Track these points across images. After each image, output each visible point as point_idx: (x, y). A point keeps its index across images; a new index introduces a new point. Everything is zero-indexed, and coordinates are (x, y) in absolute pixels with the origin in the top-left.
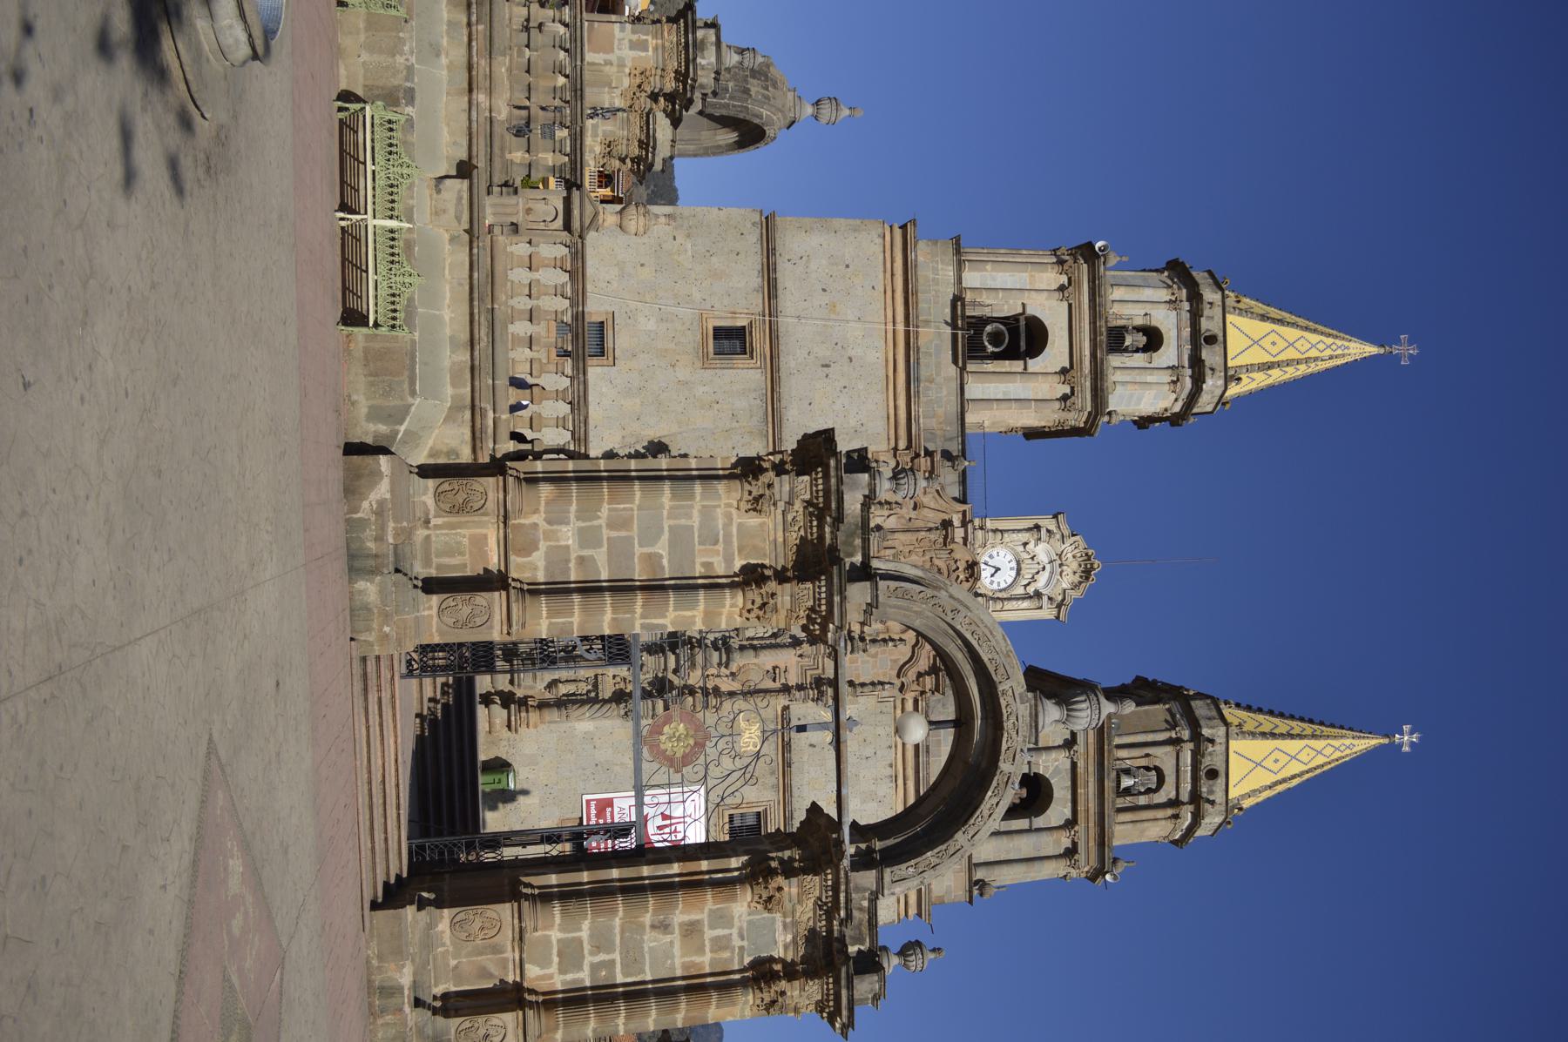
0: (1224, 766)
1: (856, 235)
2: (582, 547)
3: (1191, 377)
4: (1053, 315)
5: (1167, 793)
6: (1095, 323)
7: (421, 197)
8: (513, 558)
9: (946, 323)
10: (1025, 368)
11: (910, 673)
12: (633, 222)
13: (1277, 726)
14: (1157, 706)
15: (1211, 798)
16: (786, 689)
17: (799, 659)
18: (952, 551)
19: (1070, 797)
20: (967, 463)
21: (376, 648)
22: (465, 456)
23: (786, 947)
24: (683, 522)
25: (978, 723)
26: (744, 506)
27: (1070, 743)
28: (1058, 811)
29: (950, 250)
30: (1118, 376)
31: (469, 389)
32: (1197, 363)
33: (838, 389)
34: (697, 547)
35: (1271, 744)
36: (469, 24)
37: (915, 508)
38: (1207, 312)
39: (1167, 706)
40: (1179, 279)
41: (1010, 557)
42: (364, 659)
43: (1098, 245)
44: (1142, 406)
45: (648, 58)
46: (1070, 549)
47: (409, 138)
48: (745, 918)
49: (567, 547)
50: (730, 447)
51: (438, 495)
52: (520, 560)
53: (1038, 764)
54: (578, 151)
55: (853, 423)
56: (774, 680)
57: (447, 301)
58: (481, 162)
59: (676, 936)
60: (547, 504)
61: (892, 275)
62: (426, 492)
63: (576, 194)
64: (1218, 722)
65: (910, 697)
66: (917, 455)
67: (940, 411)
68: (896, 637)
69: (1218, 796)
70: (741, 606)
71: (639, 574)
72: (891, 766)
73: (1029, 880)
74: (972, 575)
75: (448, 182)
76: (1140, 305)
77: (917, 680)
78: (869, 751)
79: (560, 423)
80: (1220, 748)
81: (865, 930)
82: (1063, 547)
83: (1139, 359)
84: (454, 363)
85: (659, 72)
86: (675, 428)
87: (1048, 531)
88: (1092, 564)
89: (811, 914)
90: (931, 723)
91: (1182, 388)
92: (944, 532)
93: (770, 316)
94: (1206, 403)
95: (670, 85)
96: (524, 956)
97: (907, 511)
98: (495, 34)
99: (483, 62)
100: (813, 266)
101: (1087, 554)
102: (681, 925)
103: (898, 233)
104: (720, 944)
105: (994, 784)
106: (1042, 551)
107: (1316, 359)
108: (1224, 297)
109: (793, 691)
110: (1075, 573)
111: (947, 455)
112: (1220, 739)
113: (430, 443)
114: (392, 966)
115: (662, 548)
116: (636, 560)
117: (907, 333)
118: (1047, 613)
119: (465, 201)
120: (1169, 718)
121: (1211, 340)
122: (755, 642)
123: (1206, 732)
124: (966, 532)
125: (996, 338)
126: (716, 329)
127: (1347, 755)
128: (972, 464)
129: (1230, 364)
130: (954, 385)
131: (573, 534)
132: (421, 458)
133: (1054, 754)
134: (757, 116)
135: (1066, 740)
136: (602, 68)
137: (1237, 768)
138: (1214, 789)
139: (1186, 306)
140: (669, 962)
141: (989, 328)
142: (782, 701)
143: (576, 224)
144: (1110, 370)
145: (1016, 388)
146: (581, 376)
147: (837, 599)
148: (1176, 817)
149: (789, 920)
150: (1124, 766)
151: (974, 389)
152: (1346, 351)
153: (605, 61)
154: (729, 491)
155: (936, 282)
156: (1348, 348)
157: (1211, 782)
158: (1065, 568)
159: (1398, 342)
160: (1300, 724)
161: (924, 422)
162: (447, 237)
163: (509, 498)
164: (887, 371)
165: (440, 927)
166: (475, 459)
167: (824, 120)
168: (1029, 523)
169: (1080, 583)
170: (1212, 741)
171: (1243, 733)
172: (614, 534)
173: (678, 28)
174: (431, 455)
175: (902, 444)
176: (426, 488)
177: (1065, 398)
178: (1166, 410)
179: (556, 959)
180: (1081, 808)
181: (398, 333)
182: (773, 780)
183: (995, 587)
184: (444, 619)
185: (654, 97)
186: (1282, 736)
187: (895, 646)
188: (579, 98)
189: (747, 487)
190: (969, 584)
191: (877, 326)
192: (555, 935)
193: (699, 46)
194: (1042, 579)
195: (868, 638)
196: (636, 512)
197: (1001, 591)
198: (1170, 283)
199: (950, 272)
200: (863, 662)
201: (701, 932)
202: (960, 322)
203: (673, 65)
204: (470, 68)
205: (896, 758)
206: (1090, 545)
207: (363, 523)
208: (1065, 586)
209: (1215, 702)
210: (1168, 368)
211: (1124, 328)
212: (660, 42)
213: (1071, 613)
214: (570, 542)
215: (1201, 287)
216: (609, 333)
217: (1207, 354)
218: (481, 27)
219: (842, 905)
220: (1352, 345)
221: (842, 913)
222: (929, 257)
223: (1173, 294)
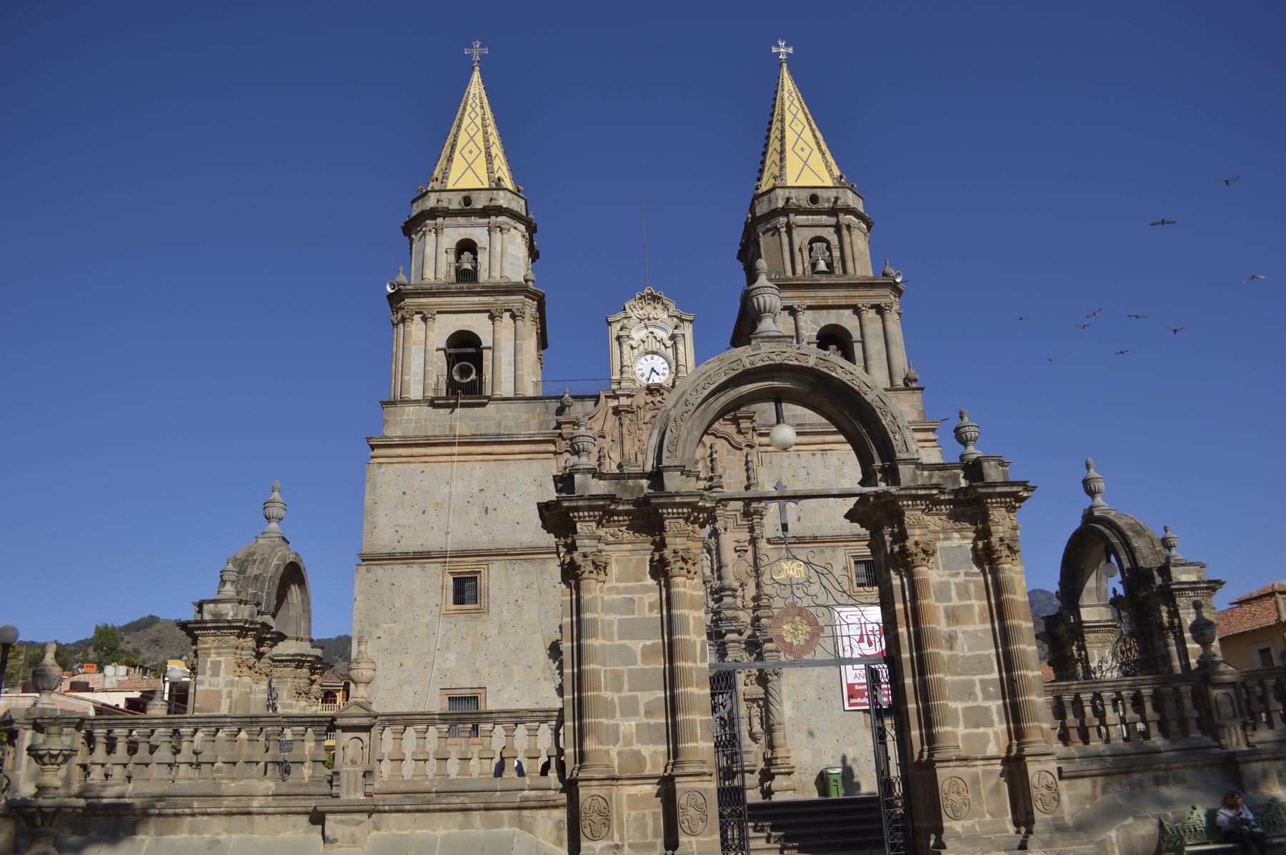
0: (807, 190)
1: (378, 486)
2: (636, 713)
3: (497, 217)
4: (446, 326)
5: (829, 234)
6: (453, 293)
8: (647, 772)
9: (452, 412)
10: (489, 348)
12: (364, 672)
13: (775, 149)
14: (761, 242)
15: (833, 200)
16: (753, 541)
19: (835, 311)
20: (567, 395)
22: (561, 814)
23: (964, 538)
24: (615, 628)
25: (776, 384)
26: (602, 577)
27: (792, 311)
28: (847, 320)
31: (504, 812)
32: (486, 212)
33: (507, 500)
34: (636, 615)
37: (603, 437)
38: (445, 204)
39: (761, 235)
40: (418, 226)
41: (642, 360)
43: (389, 290)
44: (520, 255)
45: (226, 661)
46: (636, 312)
48: (941, 571)
49: (637, 726)
50: (554, 589)
51: (594, 838)
52: (649, 766)
54: (303, 720)
55: (533, 488)
56: (746, 551)
57: (429, 832)
58: (311, 804)
59: (959, 629)
60: (601, 744)
63: (339, 722)
64: (772, 195)
66: (560, 435)
67: (524, 417)
68: (709, 451)
69: (832, 194)
71: (659, 665)
72: (814, 455)
75: (327, 832)
76: (439, 257)
79: (533, 733)
80: (794, 194)
81: (947, 473)
82: (634, 317)
83: (482, 258)
84: (483, 826)
85: (238, 651)
86: (538, 636)
87: (621, 329)
88: (648, 294)
89: (936, 518)
91: (506, 223)
92: (623, 413)
93: (446, 557)
94: (518, 205)
95: (250, 642)
96: (980, 756)
97: (606, 443)
100: (404, 522)
101: (640, 299)
102: (949, 625)
103: (378, 452)
104: (963, 592)
105: (825, 370)
106: (638, 334)
107: (483, 119)
109: (755, 535)
110: (655, 308)
111: (560, 411)
112: (787, 193)
115: (637, 646)
116: (648, 667)
117: (461, 444)
118: (687, 330)
120: (771, 233)
121: (467, 201)
122: (715, 567)
123: (781, 204)
124: (623, 395)
125: (465, 372)
126: (456, 602)
128: (567, 390)
129: (487, 186)
130: (503, 405)
131: (627, 721)
133: (801, 324)
135: (790, 314)
138: (825, 197)
139: (440, 220)
140: (979, 634)
142: (762, 544)
143: (365, 721)
144: (491, 280)
145: (505, 356)
146: (493, 716)
147: (678, 500)
148: (848, 227)
150: (809, 268)
151: (506, 389)
152: (477, 96)
153: (228, 698)
154: (589, 590)
155: (417, 421)
156: (475, 95)
157: (820, 200)
158: (651, 316)
159: (470, 56)
160: (773, 131)
162: (374, 833)
167: (282, 513)
168: (615, 344)
169: (663, 304)
170: (788, 200)
171: (781, 175)
172: (626, 686)
173: (202, 635)
174: (561, 844)
175: (551, 448)
176: (588, 848)
177: (513, 317)
178: (523, 236)
179: (982, 730)
180: (844, 302)
182: (828, 551)
183: (667, 372)
184: (699, 831)
185: (259, 656)
186: (783, 145)
187: (716, 452)
188: (258, 720)
189: (586, 575)
192: (961, 730)
193: (218, 618)
194: (660, 334)
195: (710, 474)
196: (608, 668)
197: (670, 367)
198: (421, 233)
199: (410, 409)
200: (730, 477)
201: (954, 608)
202: (451, 401)
203: (232, 640)
205: (808, 451)
206: (633, 296)
208: (665, 316)
209: (757, 197)
210: (490, 234)
211: (457, 269)
212: (213, 651)
213: (689, 311)
214: (633, 723)
215: (425, 208)
216: (458, 693)
218: (196, 805)
219: (928, 492)
220: (472, 92)
221: (934, 492)
222: (397, 426)
223: (430, 231)
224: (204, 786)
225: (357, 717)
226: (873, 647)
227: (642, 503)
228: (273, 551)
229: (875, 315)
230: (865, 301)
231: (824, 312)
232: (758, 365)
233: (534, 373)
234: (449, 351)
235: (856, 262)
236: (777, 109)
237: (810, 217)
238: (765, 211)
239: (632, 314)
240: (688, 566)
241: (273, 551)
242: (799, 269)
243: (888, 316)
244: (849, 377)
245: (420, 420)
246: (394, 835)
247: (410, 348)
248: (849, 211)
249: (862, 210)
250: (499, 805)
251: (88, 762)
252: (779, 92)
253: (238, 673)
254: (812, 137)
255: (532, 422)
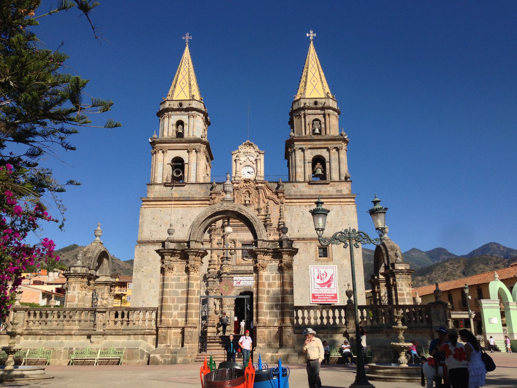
2: (177, 309)
3: (192, 111)
4: (172, 155)
5: (321, 118)
7: (94, 346)
8: (179, 326)
10: (187, 164)
11: (277, 201)
12: (105, 296)
13: (303, 81)
14: (294, 121)
15: (323, 103)
17: (271, 235)
18: (240, 187)
19: (320, 150)
20: (214, 183)
21: (193, 358)
22: (155, 336)
23: (276, 263)
24: (174, 286)
26: (171, 271)
27: (303, 150)
28: (324, 153)
29: (150, 187)
30: (191, 134)
31: (140, 336)
32: (188, 110)
34: (180, 282)
35: (308, 83)
36: (56, 335)
38: (172, 106)
39: (294, 117)
41: (244, 169)
42: (196, 361)
43: (150, 141)
44: (201, 126)
45: (78, 286)
47: (81, 349)
48: (268, 272)
49: (178, 313)
51: (162, 343)
52: (180, 324)
53: (309, 160)
57: (119, 341)
58: (87, 332)
60: (166, 318)
61: (157, 205)
62: (161, 346)
63: (97, 310)
65: (285, 201)
66: (211, 198)
67: (199, 190)
68: (266, 205)
70: (193, 272)
71: (185, 296)
72: (306, 207)
73: (347, 162)
74: (248, 181)
75: (91, 340)
77: (280, 198)
78: (301, 214)
79: (151, 314)
81: (274, 243)
82: (242, 152)
83: (186, 128)
84: (134, 339)
85: (82, 283)
87: (237, 157)
88: (247, 143)
89: (269, 256)
90: (228, 226)
91: (195, 114)
94: (200, 106)
95: (86, 280)
96: (272, 326)
98: (59, 329)
99: (65, 332)
100: (153, 229)
101: (244, 145)
102: (268, 288)
103: (144, 203)
104: (274, 279)
105: (240, 212)
106: (243, 158)
107: (189, 69)
108: (168, 100)
111: (211, 189)
113: (151, 345)
114: (266, 357)
115: (180, 291)
117: (175, 201)
118: (262, 157)
119: (96, 336)
121: (181, 105)
123: (302, 105)
127: (315, 56)
128: (214, 181)
129: (188, 99)
130: (191, 186)
132: (154, 347)
133: (306, 155)
134: (97, 254)
135: (302, 151)
136: (80, 298)
137: (315, 95)
139: (170, 113)
141: (175, 175)
143: (104, 310)
144: (189, 137)
145: (193, 167)
147: (192, 250)
148: (329, 115)
149: (269, 262)
151: (193, 180)
152: (187, 58)
153: (78, 298)
154: (167, 275)
156: (186, 58)
157: (318, 103)
158: (248, 152)
159: (185, 40)
160: (304, 72)
161: (202, 195)
162: (105, 340)
163: (163, 326)
164: (185, 207)
165: (261, 346)
166: (209, 333)
167: (101, 234)
168: (234, 163)
169: (253, 147)
170: (305, 103)
172: (176, 302)
173: (70, 278)
174: (154, 345)
175: (208, 202)
176: (160, 346)
177: (196, 152)
178: (202, 118)
180: (323, 146)
181: (123, 352)
182: (308, 244)
184: (190, 342)
185: (89, 284)
186: (306, 79)
187: (269, 205)
189: (166, 271)
190: (251, 182)
191: (172, 210)
193: (75, 272)
194: (251, 159)
195: (266, 214)
196: (171, 297)
197: (254, 172)
198: (163, 118)
199: (157, 187)
200: (274, 215)
201: (270, 283)
203: (80, 279)
204: (66, 335)
205: (304, 205)
206: (241, 144)
207: (165, 361)
208: (254, 151)
209: (295, 102)
210: (189, 118)
211: (177, 132)
214: (177, 312)
217: (185, 107)
218: (57, 332)
219: (264, 250)
220: (185, 56)
221: (266, 250)
223: (166, 117)
224: (59, 327)
225: (295, 175)
226: (322, 280)
227: (183, 251)
228: (96, 248)
229: (336, 151)
230: (331, 146)
231: (316, 150)
232: (220, 210)
233: (204, 173)
234: (172, 164)
235: (331, 129)
236: (306, 62)
237: (314, 111)
238: (297, 108)
239: (241, 151)
240: (195, 269)
241: (96, 248)
242: (308, 132)
243: (341, 151)
244: (247, 214)
245: (161, 191)
246: (110, 341)
247: (158, 163)
248: (329, 108)
249: (336, 108)
250: (138, 334)
251: (29, 320)
252: (308, 54)
253: (81, 290)
254: (319, 75)
255: (201, 192)
